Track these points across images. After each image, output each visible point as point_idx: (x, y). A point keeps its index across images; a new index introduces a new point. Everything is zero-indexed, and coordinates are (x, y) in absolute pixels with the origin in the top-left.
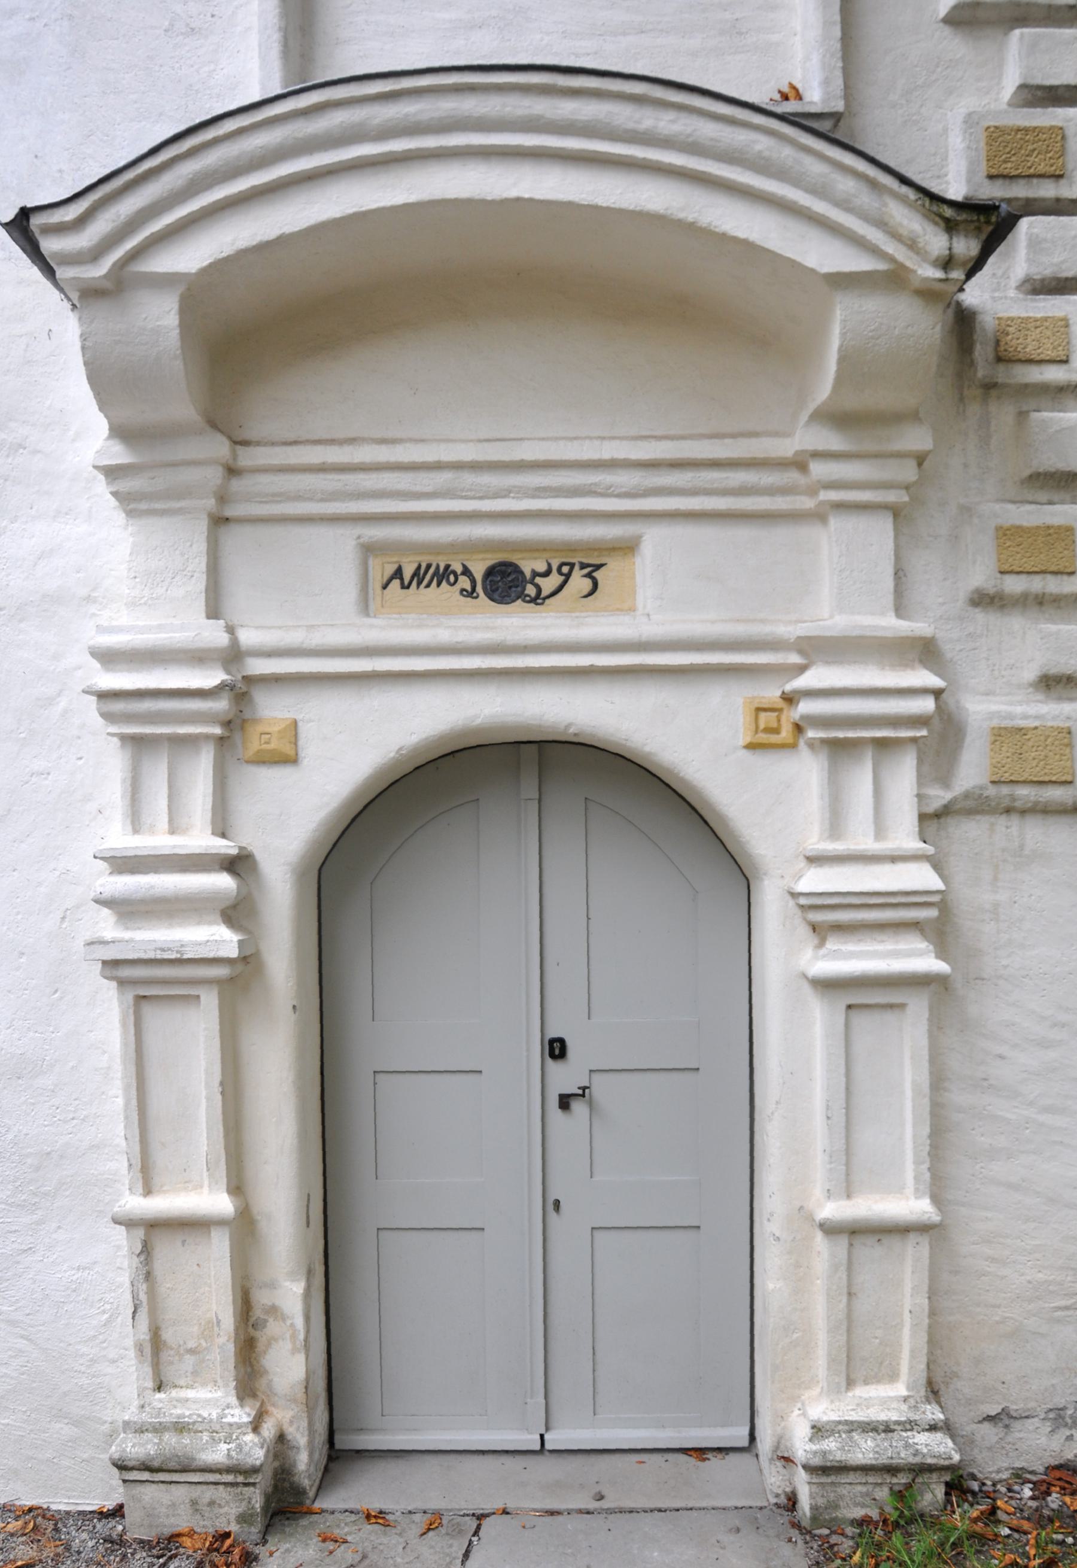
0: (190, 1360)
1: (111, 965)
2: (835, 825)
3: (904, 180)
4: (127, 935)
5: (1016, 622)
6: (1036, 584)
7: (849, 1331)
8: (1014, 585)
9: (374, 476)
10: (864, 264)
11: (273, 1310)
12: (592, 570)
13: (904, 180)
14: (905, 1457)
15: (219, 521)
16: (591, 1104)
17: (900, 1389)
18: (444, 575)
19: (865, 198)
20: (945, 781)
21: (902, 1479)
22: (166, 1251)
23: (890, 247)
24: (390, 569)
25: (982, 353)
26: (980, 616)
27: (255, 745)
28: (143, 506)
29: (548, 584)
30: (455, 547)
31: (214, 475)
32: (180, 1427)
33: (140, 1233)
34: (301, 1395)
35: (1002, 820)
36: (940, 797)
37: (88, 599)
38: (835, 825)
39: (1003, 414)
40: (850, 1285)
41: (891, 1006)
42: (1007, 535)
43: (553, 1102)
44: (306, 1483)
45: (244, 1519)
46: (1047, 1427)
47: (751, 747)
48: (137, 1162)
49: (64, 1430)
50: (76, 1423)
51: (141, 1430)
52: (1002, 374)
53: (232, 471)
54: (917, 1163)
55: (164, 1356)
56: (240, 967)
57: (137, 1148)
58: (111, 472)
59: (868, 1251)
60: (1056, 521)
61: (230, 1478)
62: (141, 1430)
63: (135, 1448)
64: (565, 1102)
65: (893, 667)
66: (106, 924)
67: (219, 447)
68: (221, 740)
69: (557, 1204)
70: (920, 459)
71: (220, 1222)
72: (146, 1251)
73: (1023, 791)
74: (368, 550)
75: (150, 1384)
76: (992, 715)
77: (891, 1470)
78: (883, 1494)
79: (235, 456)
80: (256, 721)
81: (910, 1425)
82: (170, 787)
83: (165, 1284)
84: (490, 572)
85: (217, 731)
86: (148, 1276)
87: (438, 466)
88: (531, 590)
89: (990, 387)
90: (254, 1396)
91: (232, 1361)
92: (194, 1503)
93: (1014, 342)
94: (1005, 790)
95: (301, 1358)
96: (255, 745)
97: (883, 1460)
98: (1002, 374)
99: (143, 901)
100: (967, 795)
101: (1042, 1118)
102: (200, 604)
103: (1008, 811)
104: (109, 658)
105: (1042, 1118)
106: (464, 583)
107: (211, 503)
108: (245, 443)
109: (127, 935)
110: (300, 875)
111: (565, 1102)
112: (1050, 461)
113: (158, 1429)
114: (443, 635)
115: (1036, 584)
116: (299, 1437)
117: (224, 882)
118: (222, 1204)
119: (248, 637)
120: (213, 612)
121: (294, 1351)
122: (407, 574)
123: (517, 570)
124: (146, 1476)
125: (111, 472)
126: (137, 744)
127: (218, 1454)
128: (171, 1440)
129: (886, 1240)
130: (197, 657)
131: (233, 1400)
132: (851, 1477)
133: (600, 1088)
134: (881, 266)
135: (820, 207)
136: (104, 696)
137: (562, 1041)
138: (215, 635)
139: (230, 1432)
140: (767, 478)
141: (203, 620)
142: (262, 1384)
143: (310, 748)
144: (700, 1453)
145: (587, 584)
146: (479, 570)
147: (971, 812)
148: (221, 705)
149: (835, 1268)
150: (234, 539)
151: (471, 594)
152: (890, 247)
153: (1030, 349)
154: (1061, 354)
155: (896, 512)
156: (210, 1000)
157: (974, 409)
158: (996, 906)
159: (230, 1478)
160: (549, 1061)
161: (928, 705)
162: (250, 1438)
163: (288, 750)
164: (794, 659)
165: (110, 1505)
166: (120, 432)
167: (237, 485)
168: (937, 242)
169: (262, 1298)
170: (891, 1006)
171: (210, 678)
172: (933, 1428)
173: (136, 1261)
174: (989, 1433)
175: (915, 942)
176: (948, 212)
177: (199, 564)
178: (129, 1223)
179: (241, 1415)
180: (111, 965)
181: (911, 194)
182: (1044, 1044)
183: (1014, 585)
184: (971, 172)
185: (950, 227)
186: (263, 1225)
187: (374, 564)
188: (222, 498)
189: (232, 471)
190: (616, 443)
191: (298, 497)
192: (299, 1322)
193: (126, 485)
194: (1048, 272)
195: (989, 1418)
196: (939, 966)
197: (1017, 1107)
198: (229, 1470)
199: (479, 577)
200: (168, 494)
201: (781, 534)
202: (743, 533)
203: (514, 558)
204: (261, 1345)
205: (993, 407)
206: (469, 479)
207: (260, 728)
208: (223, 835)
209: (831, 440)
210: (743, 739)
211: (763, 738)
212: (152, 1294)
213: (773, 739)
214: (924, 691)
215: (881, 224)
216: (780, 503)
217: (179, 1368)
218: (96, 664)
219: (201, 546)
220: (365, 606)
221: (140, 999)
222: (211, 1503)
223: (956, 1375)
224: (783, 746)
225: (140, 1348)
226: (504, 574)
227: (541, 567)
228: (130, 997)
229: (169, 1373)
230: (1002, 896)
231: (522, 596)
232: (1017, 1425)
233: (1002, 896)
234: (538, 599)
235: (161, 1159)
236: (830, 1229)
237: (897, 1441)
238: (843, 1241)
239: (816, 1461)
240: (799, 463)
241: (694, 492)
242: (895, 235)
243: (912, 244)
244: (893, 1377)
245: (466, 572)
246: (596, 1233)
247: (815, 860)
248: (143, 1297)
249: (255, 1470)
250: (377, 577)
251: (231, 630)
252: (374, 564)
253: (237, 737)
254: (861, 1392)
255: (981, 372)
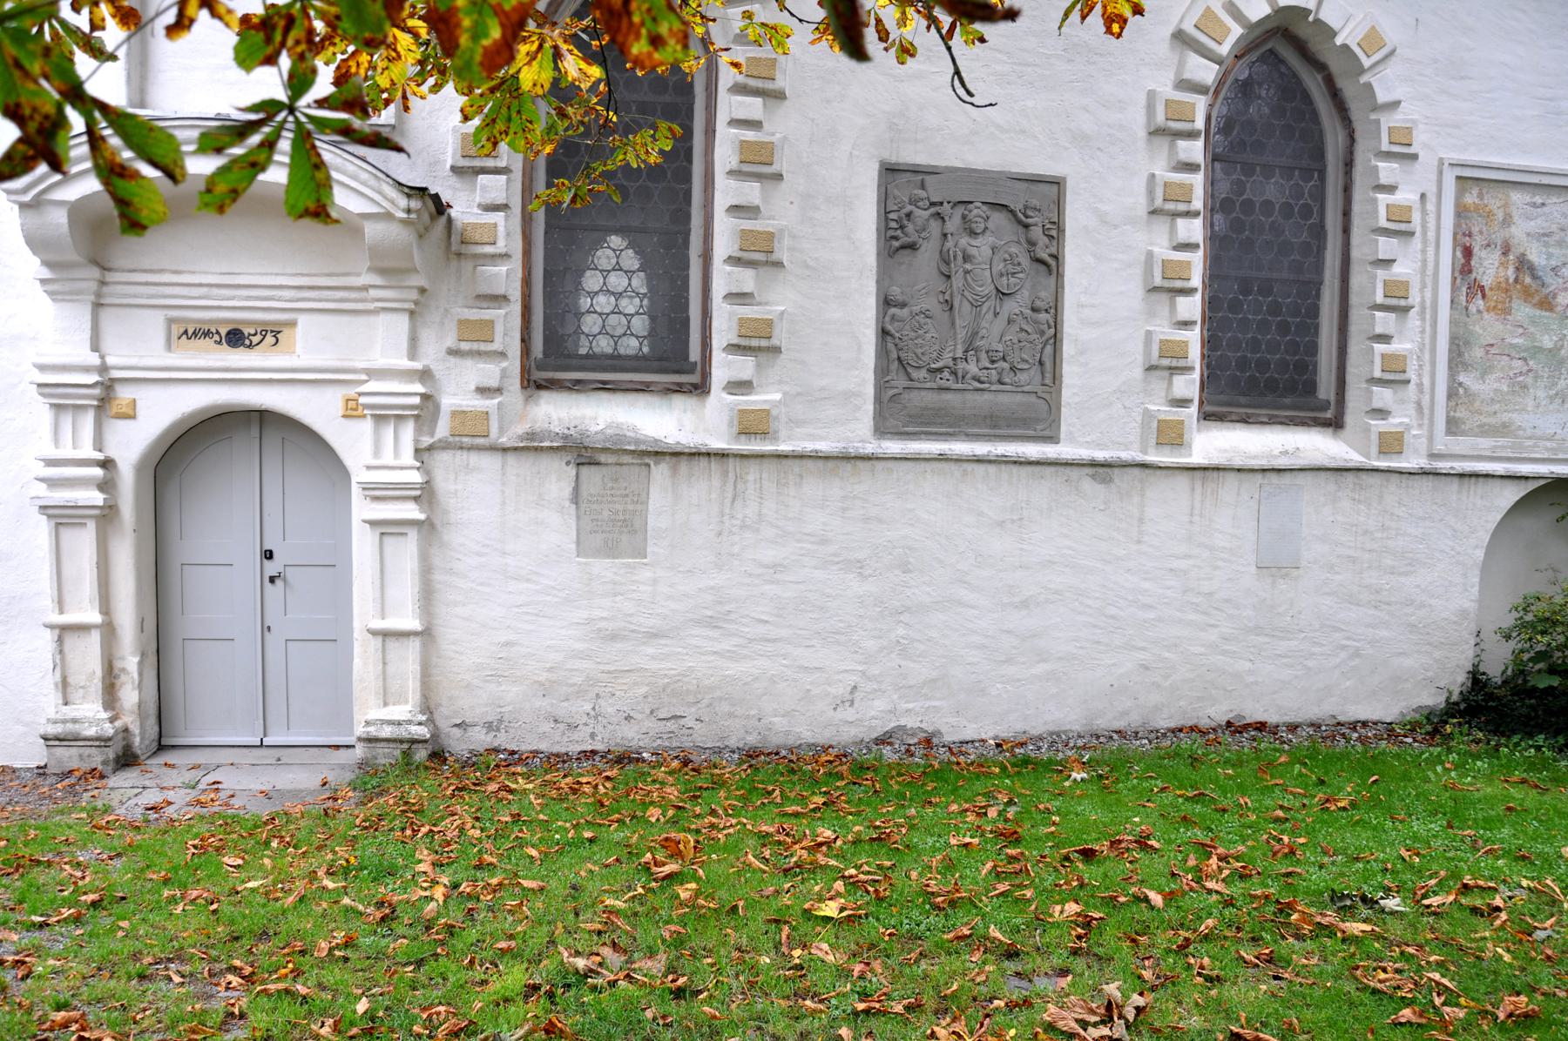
0: (81, 691)
1: (43, 508)
2: (377, 451)
3: (388, 176)
4: (50, 494)
5: (469, 363)
6: (475, 346)
7: (384, 680)
8: (465, 346)
9: (171, 288)
10: (374, 209)
11: (123, 670)
12: (276, 334)
13: (388, 176)
14: (405, 735)
15: (98, 306)
16: (285, 580)
17: (409, 707)
18: (207, 334)
19: (373, 182)
20: (432, 434)
21: (405, 746)
22: (71, 641)
23: (385, 203)
24: (182, 330)
25: (455, 239)
26: (452, 360)
27: (114, 410)
28: (59, 297)
29: (255, 340)
30: (211, 321)
31: (93, 286)
32: (74, 721)
33: (57, 632)
34: (136, 708)
35: (459, 452)
36: (426, 441)
37: (34, 338)
38: (377, 451)
39: (467, 266)
40: (384, 658)
41: (402, 534)
42: (463, 324)
43: (267, 580)
44: (139, 752)
45: (105, 763)
46: (484, 731)
47: (344, 416)
48: (56, 599)
49: (22, 729)
50: (27, 725)
51: (55, 722)
52: (464, 249)
53: (103, 283)
54: (414, 604)
55: (69, 690)
56: (106, 512)
57: (56, 593)
58: (43, 281)
59: (392, 644)
60: (487, 317)
61: (97, 743)
62: (55, 722)
63: (53, 730)
64: (272, 580)
65: (406, 382)
66: (41, 490)
67: (95, 273)
68: (98, 407)
69: (269, 628)
70: (423, 291)
71: (96, 626)
72: (60, 640)
73: (465, 440)
74: (171, 321)
75: (61, 702)
76: (451, 405)
77: (401, 741)
78: (397, 753)
79: (104, 276)
80: (115, 399)
81: (409, 722)
82: (74, 427)
83: (70, 656)
84: (229, 333)
85: (95, 403)
86: (61, 652)
87: (201, 285)
88: (247, 342)
89: (459, 255)
90: (113, 709)
91: (100, 692)
92: (80, 756)
93: (469, 234)
94: (457, 439)
95: (137, 692)
96: (114, 410)
97: (395, 736)
98: (464, 249)
99: (59, 480)
100: (440, 441)
101: (479, 588)
102: (88, 344)
103: (461, 448)
104: (42, 368)
105: (479, 588)
106: (217, 338)
107: (92, 298)
108: (109, 270)
109: (50, 494)
110: (140, 468)
111: (272, 580)
112: (485, 289)
113: (64, 722)
114: (202, 363)
115: (475, 346)
116: (135, 729)
117: (98, 472)
118: (95, 617)
119: (110, 360)
120: (95, 347)
121: (133, 689)
122: (190, 333)
123: (241, 332)
124: (57, 743)
125: (43, 281)
126: (58, 408)
127: (91, 732)
128: (70, 726)
129: (401, 639)
130: (86, 369)
131: (101, 709)
132: (383, 744)
133: (290, 573)
134: (382, 211)
135: (354, 184)
136: (40, 385)
137: (271, 552)
138: (94, 360)
139: (98, 722)
140: (353, 295)
141: (89, 352)
142: (118, 705)
143: (141, 411)
144: (337, 747)
145: (274, 340)
146: (223, 332)
147: (444, 448)
148: (97, 391)
149: (377, 650)
150: (107, 316)
151: (220, 343)
152: (385, 203)
153: (477, 238)
154: (492, 240)
155: (412, 313)
156: (91, 525)
157: (454, 263)
158: (456, 491)
159: (97, 743)
160: (265, 561)
161: (417, 400)
162: (107, 725)
163: (131, 412)
164: (364, 377)
165: (42, 764)
166: (46, 263)
167: (105, 289)
168: (403, 202)
169: (118, 664)
170: (402, 534)
171: (93, 378)
172: (420, 724)
173: (55, 645)
174: (457, 732)
175: (412, 506)
176: (406, 190)
177: (87, 325)
178: (52, 627)
179: (105, 715)
180: (43, 508)
181: (391, 182)
182: (479, 554)
183: (465, 346)
184: (454, 154)
185: (409, 196)
186: (119, 631)
187: (174, 327)
188: (98, 295)
189: (103, 283)
190: (282, 278)
191: (135, 296)
192: (136, 675)
193: (50, 287)
194: (489, 201)
195: (456, 725)
196: (422, 517)
197: (633, 631)
198: (97, 739)
199: (223, 335)
200: (71, 293)
201: (361, 320)
202: (345, 319)
203: (240, 327)
204: (117, 687)
205: (463, 263)
206: (215, 291)
207: (118, 402)
208: (100, 451)
209: (378, 280)
210: (341, 413)
211: (349, 412)
212: (63, 660)
213: (355, 413)
214: (416, 394)
215: (380, 193)
216: (360, 306)
217: (75, 695)
218: (36, 371)
219: (88, 317)
220: (169, 346)
221: (58, 525)
222: (89, 756)
223: (440, 705)
224: (359, 417)
225: (56, 685)
226: (235, 334)
227: (253, 332)
228: (53, 523)
229: (71, 697)
230: (460, 487)
231: (243, 344)
232: (470, 729)
233: (460, 487)
234: (250, 346)
235: (67, 598)
236: (374, 633)
237: (402, 728)
238: (380, 639)
239: (364, 736)
240: (365, 288)
241: (320, 300)
242: (385, 197)
243: (392, 202)
244: (406, 702)
245: (218, 332)
246: (289, 643)
247: (369, 468)
248: (58, 661)
249: (109, 739)
250: (175, 333)
251: (102, 357)
252: (174, 327)
253: (107, 406)
254: (390, 708)
255: (454, 248)
